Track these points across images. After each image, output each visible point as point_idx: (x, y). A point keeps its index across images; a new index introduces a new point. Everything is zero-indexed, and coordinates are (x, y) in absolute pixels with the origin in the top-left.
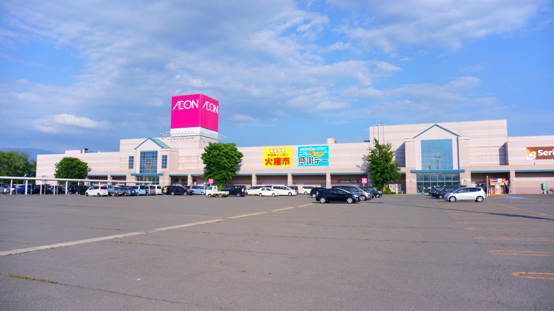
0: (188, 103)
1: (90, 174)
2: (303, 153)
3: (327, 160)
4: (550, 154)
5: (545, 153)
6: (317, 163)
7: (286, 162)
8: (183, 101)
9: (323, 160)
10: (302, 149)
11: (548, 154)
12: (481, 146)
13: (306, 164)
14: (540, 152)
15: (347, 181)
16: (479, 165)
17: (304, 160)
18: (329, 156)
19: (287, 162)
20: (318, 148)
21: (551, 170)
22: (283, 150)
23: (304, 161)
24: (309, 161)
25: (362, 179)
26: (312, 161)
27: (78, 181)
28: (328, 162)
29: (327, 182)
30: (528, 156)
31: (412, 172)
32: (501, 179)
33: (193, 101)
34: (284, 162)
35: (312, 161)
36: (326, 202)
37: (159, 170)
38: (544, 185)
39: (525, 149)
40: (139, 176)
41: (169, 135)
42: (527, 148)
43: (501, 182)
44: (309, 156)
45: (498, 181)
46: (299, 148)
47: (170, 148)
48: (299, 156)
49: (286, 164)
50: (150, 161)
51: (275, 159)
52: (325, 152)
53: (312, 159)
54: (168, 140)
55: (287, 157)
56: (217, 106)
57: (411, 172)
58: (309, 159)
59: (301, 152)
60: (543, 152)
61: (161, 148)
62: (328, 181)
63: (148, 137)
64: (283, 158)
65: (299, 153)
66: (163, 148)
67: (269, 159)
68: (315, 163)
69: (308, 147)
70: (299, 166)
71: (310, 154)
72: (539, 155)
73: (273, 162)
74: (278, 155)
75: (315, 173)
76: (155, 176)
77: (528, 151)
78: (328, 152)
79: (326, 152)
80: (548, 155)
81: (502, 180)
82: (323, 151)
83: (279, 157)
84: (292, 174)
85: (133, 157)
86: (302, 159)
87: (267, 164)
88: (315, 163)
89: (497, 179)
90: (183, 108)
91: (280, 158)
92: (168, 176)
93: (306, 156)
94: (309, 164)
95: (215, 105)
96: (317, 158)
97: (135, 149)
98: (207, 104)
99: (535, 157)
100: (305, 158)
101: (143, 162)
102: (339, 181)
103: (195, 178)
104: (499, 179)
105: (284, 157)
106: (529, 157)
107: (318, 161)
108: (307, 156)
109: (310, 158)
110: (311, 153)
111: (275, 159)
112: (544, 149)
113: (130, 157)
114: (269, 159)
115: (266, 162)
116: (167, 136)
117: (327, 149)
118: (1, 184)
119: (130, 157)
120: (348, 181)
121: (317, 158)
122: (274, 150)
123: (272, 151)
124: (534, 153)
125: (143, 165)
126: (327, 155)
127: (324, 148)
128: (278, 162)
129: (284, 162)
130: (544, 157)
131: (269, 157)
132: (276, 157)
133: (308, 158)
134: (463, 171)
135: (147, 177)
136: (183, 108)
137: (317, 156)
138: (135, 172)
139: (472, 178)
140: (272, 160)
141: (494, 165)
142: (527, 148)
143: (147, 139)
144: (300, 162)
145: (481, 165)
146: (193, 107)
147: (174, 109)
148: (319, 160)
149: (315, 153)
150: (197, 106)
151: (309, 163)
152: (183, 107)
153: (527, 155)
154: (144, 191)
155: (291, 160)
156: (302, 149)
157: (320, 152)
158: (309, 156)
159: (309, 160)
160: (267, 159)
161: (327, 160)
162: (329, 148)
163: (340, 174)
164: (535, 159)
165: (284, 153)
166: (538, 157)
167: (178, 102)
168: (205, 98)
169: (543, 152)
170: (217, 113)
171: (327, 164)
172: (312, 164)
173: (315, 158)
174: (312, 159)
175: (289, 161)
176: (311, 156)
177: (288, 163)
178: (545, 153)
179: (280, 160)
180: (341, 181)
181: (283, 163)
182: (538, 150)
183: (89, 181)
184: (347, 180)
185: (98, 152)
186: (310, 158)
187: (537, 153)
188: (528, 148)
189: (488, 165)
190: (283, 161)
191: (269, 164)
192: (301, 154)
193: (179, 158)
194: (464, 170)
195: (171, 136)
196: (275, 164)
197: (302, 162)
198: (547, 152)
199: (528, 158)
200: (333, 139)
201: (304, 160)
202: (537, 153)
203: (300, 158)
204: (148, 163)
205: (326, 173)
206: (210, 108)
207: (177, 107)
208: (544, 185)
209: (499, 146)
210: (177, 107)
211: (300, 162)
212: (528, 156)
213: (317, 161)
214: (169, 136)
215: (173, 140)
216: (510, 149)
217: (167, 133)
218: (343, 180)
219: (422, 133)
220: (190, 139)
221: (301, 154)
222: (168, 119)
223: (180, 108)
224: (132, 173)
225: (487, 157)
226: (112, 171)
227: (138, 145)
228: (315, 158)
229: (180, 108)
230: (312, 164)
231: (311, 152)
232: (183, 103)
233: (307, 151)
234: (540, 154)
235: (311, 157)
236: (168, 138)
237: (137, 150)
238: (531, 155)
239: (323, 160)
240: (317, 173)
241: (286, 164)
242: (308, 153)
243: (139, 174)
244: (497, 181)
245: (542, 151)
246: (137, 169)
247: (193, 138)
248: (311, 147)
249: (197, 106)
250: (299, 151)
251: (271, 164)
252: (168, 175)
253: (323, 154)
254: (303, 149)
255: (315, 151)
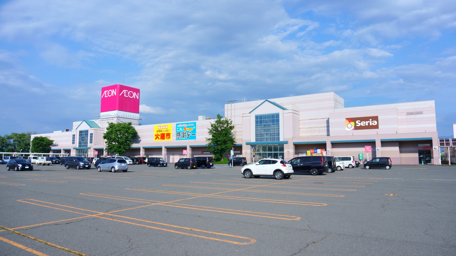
0: (110, 92)
1: (53, 148)
2: (179, 129)
3: (195, 135)
4: (367, 125)
5: (363, 124)
6: (188, 137)
7: (168, 137)
8: (128, 91)
9: (192, 135)
10: (179, 126)
11: (365, 124)
12: (311, 118)
13: (181, 138)
14: (359, 124)
15: (208, 153)
16: (310, 137)
17: (180, 134)
18: (197, 130)
19: (169, 136)
20: (189, 124)
21: (419, 138)
22: (166, 127)
23: (180, 136)
24: (183, 136)
25: (183, 150)
26: (185, 136)
27: (3, 154)
28: (196, 136)
29: (377, 150)
30: (347, 126)
31: (247, 144)
32: (320, 150)
33: (113, 90)
34: (167, 137)
35: (185, 136)
36: (370, 168)
37: (89, 145)
38: (361, 155)
39: (345, 120)
40: (80, 150)
41: (99, 117)
42: (346, 119)
43: (320, 152)
44: (183, 131)
45: (318, 152)
46: (177, 124)
47: (100, 128)
48: (176, 131)
49: (168, 139)
50: (84, 138)
51: (161, 134)
52: (194, 128)
53: (185, 134)
54: (99, 121)
55: (169, 132)
56: (138, 93)
57: (74, 149)
58: (183, 133)
59: (178, 128)
60: (360, 122)
61: (90, 127)
62: (378, 149)
63: (83, 120)
64: (166, 134)
65: (176, 129)
66: (91, 127)
67: (157, 134)
68: (187, 137)
69: (182, 124)
70: (176, 140)
71: (184, 129)
72: (357, 125)
73: (160, 137)
74: (163, 131)
75: (170, 146)
76: (266, 145)
77: (347, 122)
78: (196, 127)
79: (194, 127)
80: (365, 125)
81: (321, 150)
82: (192, 127)
83: (164, 133)
84: (165, 146)
85: (74, 135)
86: (178, 134)
87: (156, 139)
88: (187, 137)
89: (317, 150)
90: (107, 96)
91: (164, 134)
92: (93, 149)
93: (181, 132)
94: (183, 138)
95: (135, 93)
96: (188, 133)
97: (76, 129)
98: (125, 92)
99: (353, 127)
100: (180, 133)
101: (86, 139)
102: (202, 152)
103: (102, 152)
104: (318, 150)
105: (167, 133)
106: (348, 128)
107: (189, 135)
108: (182, 131)
109: (184, 133)
110: (185, 129)
111: (161, 134)
112: (362, 119)
113: (73, 135)
114: (157, 134)
115: (156, 137)
116: (98, 118)
117: (195, 125)
118: (1, 155)
119: (73, 135)
120: (208, 152)
121: (188, 133)
122: (160, 127)
123: (159, 128)
124: (353, 123)
125: (81, 141)
126: (195, 130)
127: (189, 124)
128: (163, 137)
129: (167, 137)
130: (361, 128)
131: (157, 133)
132: (162, 133)
133: (182, 133)
134: (287, 143)
135: (261, 146)
136: (107, 96)
137: (188, 131)
138: (250, 140)
139: (192, 151)
140: (159, 135)
141: (322, 136)
142: (346, 119)
143: (82, 121)
144: (177, 137)
145: (311, 137)
146: (113, 95)
147: (102, 97)
148: (190, 135)
149: (187, 129)
150: (115, 94)
151: (183, 137)
152: (127, 95)
153: (346, 126)
154: (309, 154)
155: (171, 135)
156: (179, 126)
157: (190, 128)
158: (183, 131)
159: (183, 135)
160: (156, 134)
161: (195, 135)
162: (197, 124)
163: (180, 147)
164: (353, 130)
165: (167, 129)
166: (356, 128)
167: (124, 90)
168: (122, 88)
169: (360, 122)
170: (138, 98)
171: (195, 138)
172: (185, 138)
173: (187, 133)
174: (185, 134)
175: (170, 136)
176: (185, 132)
177: (170, 138)
178: (363, 124)
179: (165, 135)
180: (204, 152)
181: (166, 138)
182: (356, 121)
183: (33, 154)
184: (208, 152)
185: (54, 132)
186: (184, 133)
187: (356, 124)
188: (347, 119)
189: (314, 137)
190: (166, 136)
191: (157, 139)
192: (178, 129)
193: (300, 130)
194: (288, 142)
195: (100, 118)
196: (161, 139)
197: (178, 137)
198: (365, 122)
199: (347, 129)
200: (202, 116)
201: (180, 134)
202: (356, 124)
203: (177, 133)
204: (258, 134)
205: (326, 141)
206: (129, 95)
207: (123, 94)
208: (360, 156)
209: (326, 118)
210: (123, 94)
211: (177, 137)
212: (347, 126)
213: (188, 136)
214: (99, 118)
215: (102, 121)
216: (330, 121)
217: (95, 116)
218: (205, 152)
219: (256, 108)
220: (111, 120)
221: (178, 129)
222: (99, 105)
223: (125, 96)
224: (74, 147)
225: (316, 129)
226: (148, 143)
227: (77, 127)
228: (187, 133)
229: (125, 96)
230: (185, 138)
231: (185, 128)
232: (128, 92)
233: (182, 127)
234: (358, 124)
235: (185, 133)
236: (99, 120)
237: (77, 130)
238: (349, 125)
239: (192, 135)
240: (171, 146)
241: (168, 139)
242: (183, 129)
243: (78, 148)
244: (317, 152)
245: (359, 121)
246: (77, 145)
247: (113, 119)
248: (184, 124)
249: (115, 94)
250: (177, 127)
251: (159, 139)
252: (93, 149)
253: (192, 129)
254: (179, 125)
255: (188, 127)
